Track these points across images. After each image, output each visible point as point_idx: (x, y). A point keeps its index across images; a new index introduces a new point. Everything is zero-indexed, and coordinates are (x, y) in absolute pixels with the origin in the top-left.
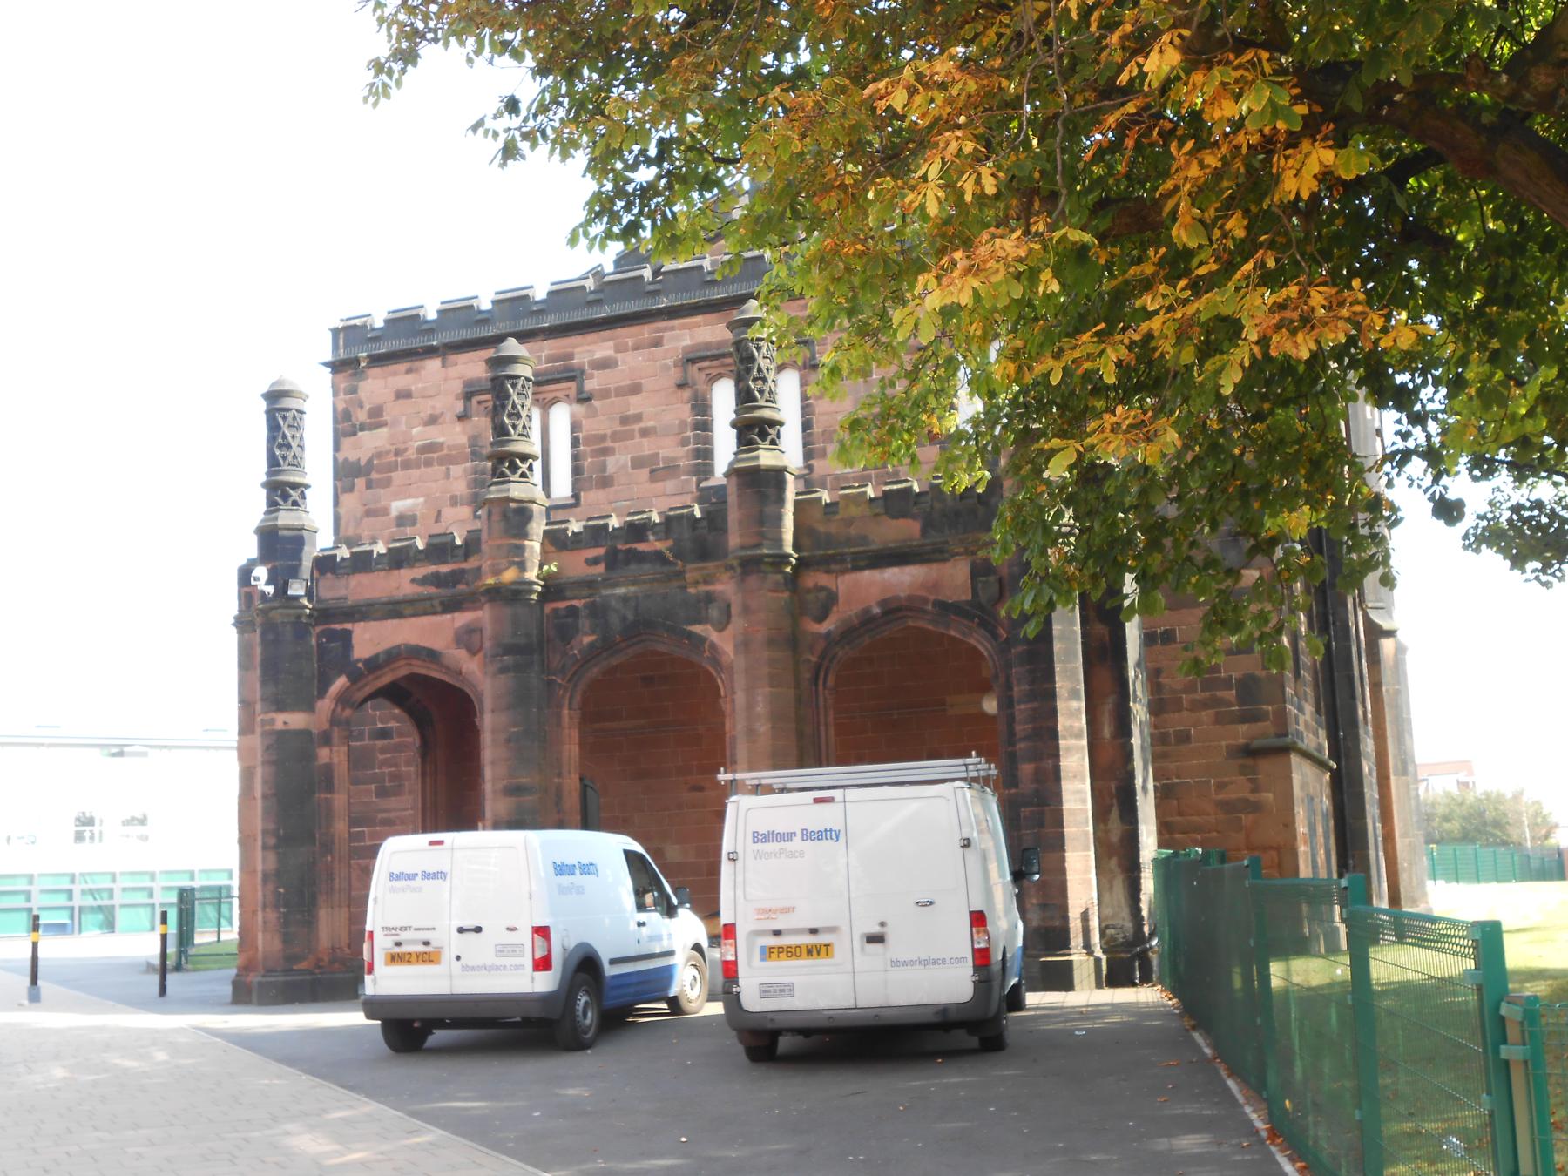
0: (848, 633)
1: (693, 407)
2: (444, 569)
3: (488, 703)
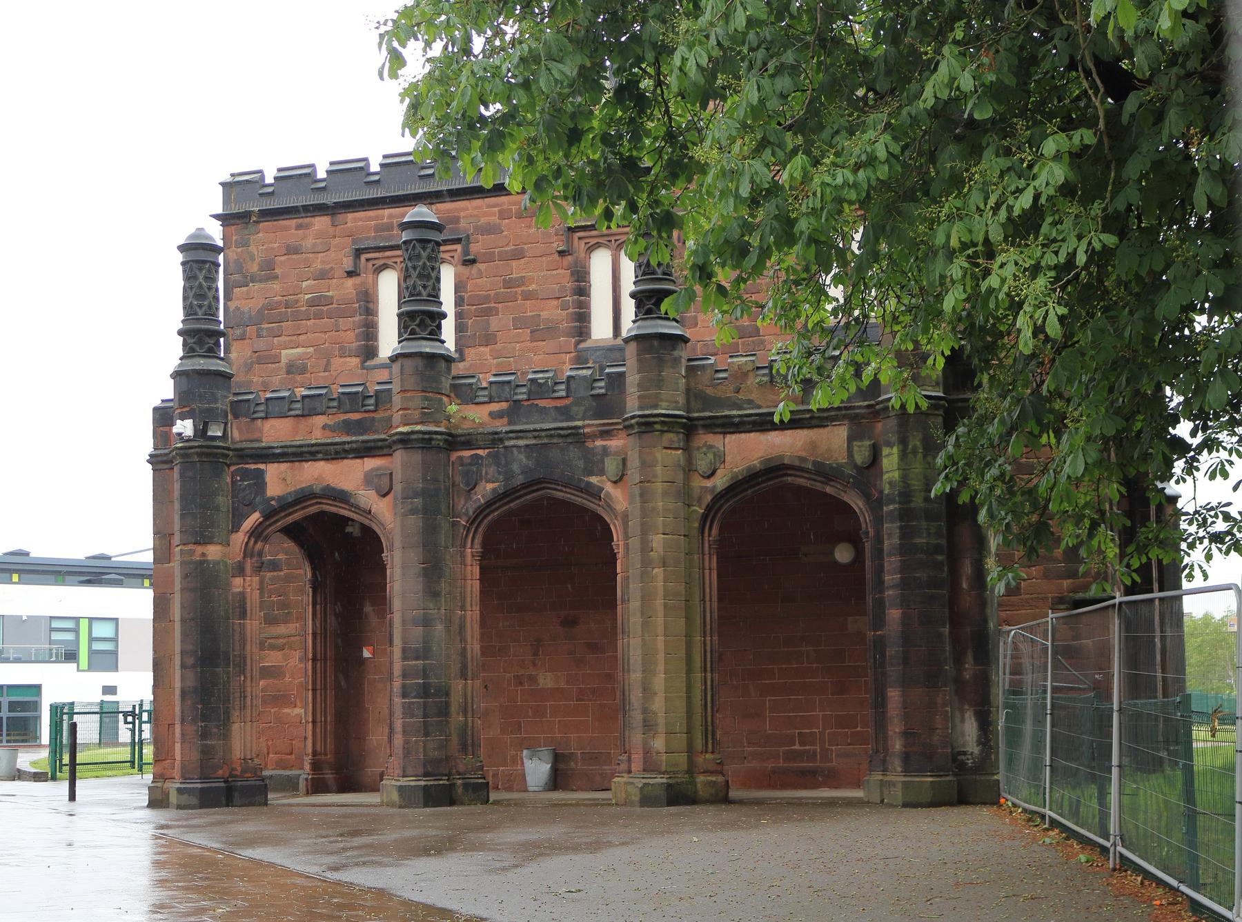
0: (735, 487)
1: (572, 274)
2: (355, 416)
3: (398, 544)
